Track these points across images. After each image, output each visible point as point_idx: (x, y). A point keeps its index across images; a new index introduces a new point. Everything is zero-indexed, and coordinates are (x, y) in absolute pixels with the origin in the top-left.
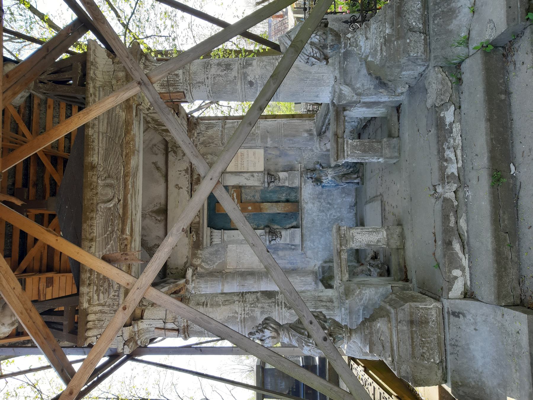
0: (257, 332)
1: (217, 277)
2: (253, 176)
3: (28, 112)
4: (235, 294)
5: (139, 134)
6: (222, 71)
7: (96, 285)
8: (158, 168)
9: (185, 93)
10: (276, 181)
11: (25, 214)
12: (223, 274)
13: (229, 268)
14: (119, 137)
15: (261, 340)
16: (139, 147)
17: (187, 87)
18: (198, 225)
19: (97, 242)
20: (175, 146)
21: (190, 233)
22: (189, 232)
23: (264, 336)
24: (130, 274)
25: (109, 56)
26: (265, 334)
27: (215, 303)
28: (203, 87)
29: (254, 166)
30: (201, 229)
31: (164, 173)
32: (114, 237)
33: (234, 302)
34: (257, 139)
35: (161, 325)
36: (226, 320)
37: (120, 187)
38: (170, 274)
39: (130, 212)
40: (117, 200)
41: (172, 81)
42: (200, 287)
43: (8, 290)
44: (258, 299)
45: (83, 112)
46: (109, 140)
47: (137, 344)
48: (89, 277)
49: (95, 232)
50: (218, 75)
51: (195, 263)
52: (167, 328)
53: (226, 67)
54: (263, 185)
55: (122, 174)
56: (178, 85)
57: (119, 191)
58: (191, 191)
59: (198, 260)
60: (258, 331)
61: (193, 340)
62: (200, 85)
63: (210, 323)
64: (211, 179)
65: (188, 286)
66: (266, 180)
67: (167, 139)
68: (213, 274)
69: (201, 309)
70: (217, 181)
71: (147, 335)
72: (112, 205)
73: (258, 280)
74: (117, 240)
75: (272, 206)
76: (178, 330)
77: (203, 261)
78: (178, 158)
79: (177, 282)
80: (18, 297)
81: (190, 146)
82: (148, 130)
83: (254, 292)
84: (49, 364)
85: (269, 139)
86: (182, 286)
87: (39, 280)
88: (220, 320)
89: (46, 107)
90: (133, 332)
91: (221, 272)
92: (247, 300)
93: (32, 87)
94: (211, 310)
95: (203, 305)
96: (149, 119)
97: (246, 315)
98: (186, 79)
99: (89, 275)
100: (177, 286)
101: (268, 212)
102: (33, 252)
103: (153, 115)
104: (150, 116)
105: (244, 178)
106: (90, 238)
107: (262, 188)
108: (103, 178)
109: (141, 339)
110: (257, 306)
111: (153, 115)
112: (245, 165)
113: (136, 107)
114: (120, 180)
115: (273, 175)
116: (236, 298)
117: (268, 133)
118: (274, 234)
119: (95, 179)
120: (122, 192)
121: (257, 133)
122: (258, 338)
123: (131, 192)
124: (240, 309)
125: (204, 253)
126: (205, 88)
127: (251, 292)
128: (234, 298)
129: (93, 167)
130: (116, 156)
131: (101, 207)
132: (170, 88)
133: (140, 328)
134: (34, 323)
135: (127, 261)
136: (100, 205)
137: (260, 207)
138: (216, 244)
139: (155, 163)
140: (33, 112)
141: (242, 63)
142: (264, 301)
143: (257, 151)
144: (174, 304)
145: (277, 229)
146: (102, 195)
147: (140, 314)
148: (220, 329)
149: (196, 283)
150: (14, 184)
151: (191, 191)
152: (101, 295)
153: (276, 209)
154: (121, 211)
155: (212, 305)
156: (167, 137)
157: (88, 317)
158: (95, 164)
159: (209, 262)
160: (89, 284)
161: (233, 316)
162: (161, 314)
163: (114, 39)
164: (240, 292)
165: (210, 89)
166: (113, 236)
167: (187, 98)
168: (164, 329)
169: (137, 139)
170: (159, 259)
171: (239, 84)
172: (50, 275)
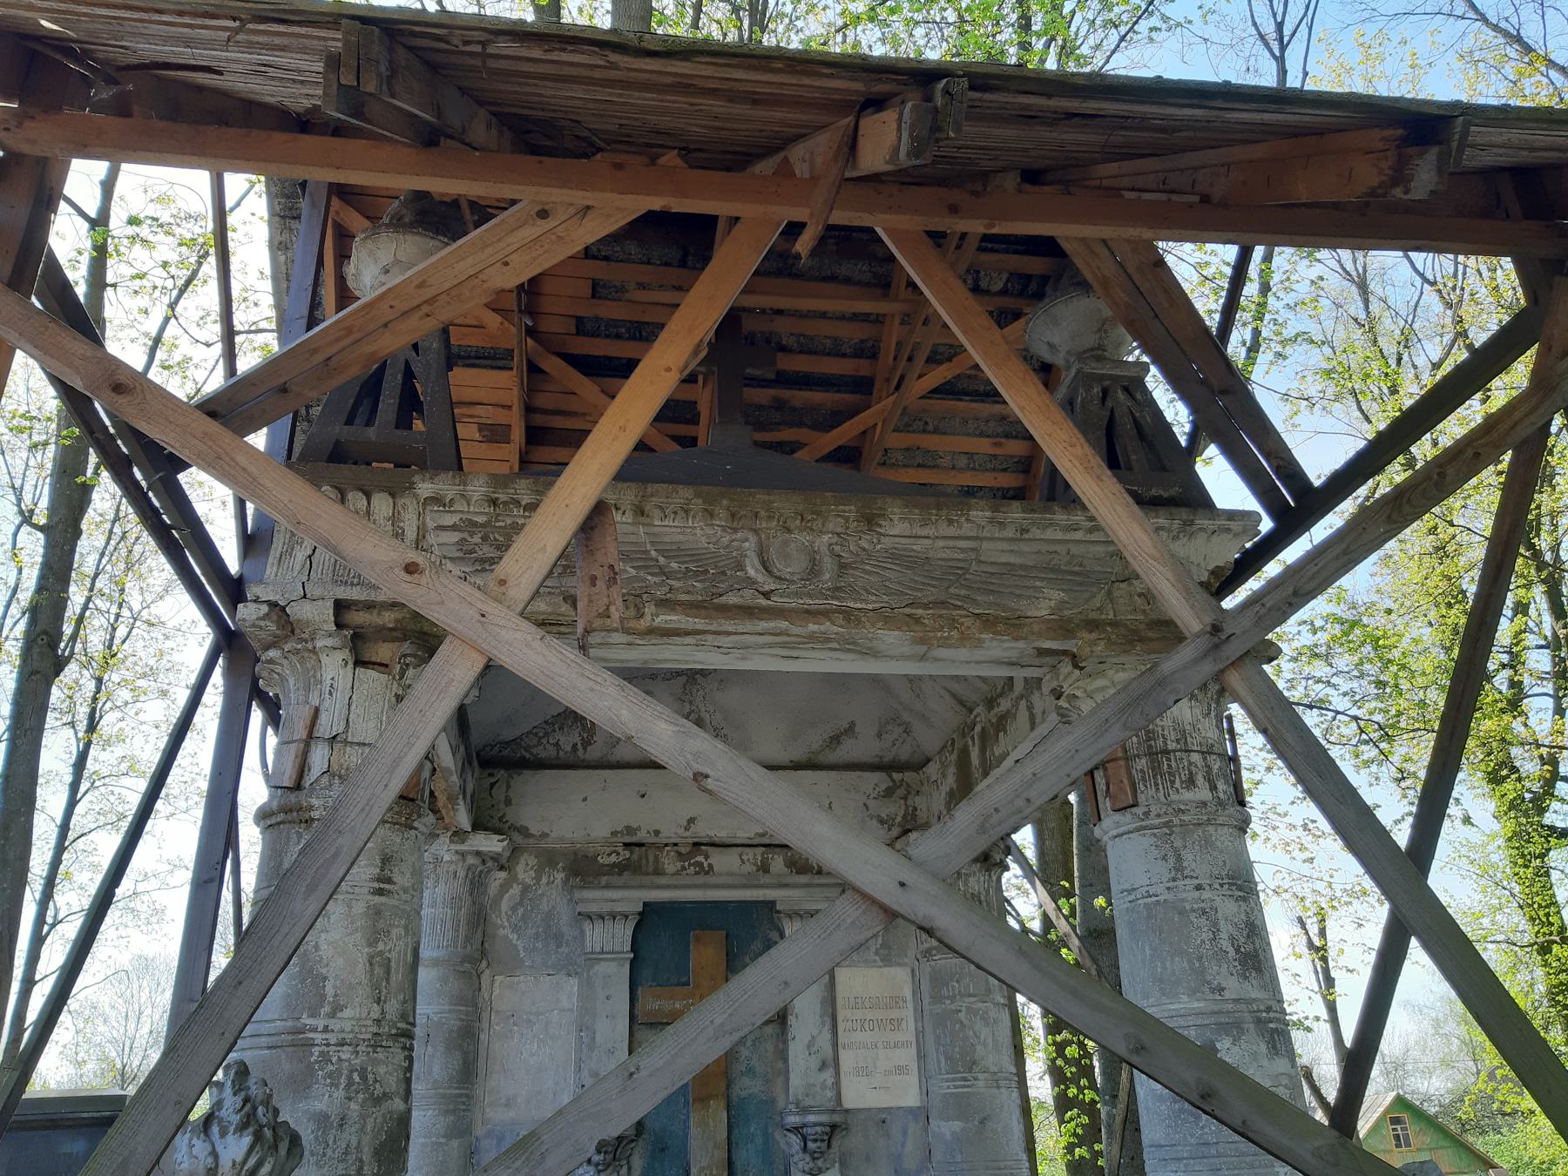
0: (246, 1100)
1: (468, 939)
2: (823, 1066)
3: (982, 388)
4: (409, 1006)
5: (977, 662)
6: (1232, 939)
7: (489, 522)
8: (835, 740)
9: (1134, 810)
10: (808, 1158)
11: (703, 369)
12: (475, 962)
13: (497, 984)
14: (968, 597)
15: (208, 1120)
16: (937, 659)
17: (1158, 816)
18: (651, 869)
19: (631, 529)
20: (909, 793)
21: (625, 845)
22: (628, 839)
23: (223, 1134)
24: (536, 594)
25: (1215, 572)
26: (230, 1138)
27: (381, 925)
28: (1163, 870)
29: (863, 1071)
30: (639, 879)
31: (821, 758)
32: (649, 577)
33: (378, 1001)
34: (954, 1080)
35: (325, 727)
36: (311, 971)
37: (811, 598)
38: (493, 780)
39: (728, 626)
40: (767, 588)
41: (1170, 766)
42: (437, 881)
43: (502, 244)
44: (377, 1101)
45: (1090, 458)
46: (958, 568)
47: (267, 648)
48: (517, 503)
49: (666, 523)
50: (1215, 924)
51: (522, 861)
52: (313, 748)
53: (1247, 955)
54: (792, 1107)
55: (851, 605)
56: (1156, 785)
57: (797, 594)
58: (764, 846)
59: (532, 873)
60: (248, 1106)
61: (250, 837)
62: (1172, 861)
63: (312, 889)
64: (902, 884)
65: (444, 839)
66: (811, 1118)
67: (932, 769)
68: (478, 924)
69: (364, 872)
70: (895, 907)
71: (297, 680)
72: (751, 572)
73: (443, 1096)
74: (636, 585)
75: (716, 1146)
76: (298, 786)
77: (526, 889)
78: (871, 803)
79: (464, 798)
80: (475, 276)
81: (1020, 802)
82: (958, 708)
83: (408, 1081)
84: (239, 373)
85: (957, 1125)
86: (447, 821)
87: (503, 407)
88: (317, 947)
89: (997, 436)
90: (314, 633)
91: (484, 954)
92: (381, 1056)
93: (1087, 370)
94: (360, 908)
95: (379, 880)
96: (1005, 704)
97: (322, 1053)
98: (1183, 812)
99: (523, 503)
100: (452, 799)
101: (694, 1131)
102: (587, 388)
103: (1023, 714)
104: (1016, 705)
105: (815, 1032)
106: (647, 508)
107: (781, 1103)
108: (837, 548)
109: (285, 662)
110: (350, 1099)
111: (1023, 714)
112: (860, 1036)
113: (1065, 652)
114: (833, 598)
115: (829, 1146)
116: (393, 1007)
117: (981, 1122)
118: (609, 1157)
119: (834, 524)
120: (793, 603)
121: (976, 1079)
122: (217, 1105)
123: (795, 630)
124: (348, 1026)
125: (553, 894)
126: (1164, 879)
127: (410, 1069)
128: (394, 1001)
129: (870, 521)
130: (911, 588)
131: (746, 540)
132: (1144, 761)
133: (323, 657)
134: (386, 325)
135: (588, 583)
136: (753, 538)
137: (710, 1097)
138: (582, 933)
139: (850, 730)
140: (983, 401)
141: (1272, 1015)
142: (369, 1128)
143: (913, 1079)
144: (410, 745)
145: (630, 1169)
146: (786, 543)
147: (373, 659)
148: (279, 937)
149: (453, 867)
150: (783, 349)
151: (764, 846)
152: (454, 537)
153: (704, 1164)
154: (732, 599)
155: (377, 912)
156: (938, 766)
157: (385, 495)
158: (880, 526)
159: (521, 911)
160: (494, 502)
161: (323, 997)
162: (364, 729)
163: (1345, 553)
164: (413, 1025)
165: (1161, 898)
166: (652, 574)
167: (1118, 817)
168: (310, 735)
169: (962, 653)
170: (592, 690)
171: (1196, 1005)
172: (518, 434)
